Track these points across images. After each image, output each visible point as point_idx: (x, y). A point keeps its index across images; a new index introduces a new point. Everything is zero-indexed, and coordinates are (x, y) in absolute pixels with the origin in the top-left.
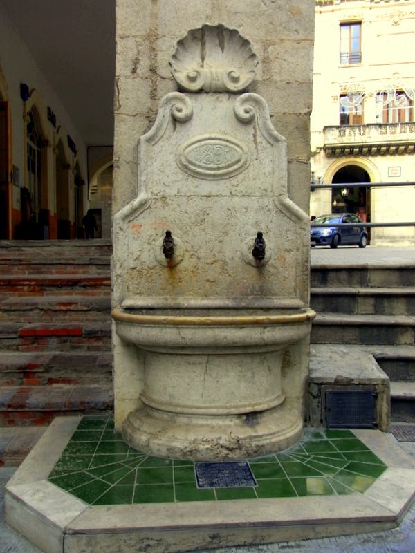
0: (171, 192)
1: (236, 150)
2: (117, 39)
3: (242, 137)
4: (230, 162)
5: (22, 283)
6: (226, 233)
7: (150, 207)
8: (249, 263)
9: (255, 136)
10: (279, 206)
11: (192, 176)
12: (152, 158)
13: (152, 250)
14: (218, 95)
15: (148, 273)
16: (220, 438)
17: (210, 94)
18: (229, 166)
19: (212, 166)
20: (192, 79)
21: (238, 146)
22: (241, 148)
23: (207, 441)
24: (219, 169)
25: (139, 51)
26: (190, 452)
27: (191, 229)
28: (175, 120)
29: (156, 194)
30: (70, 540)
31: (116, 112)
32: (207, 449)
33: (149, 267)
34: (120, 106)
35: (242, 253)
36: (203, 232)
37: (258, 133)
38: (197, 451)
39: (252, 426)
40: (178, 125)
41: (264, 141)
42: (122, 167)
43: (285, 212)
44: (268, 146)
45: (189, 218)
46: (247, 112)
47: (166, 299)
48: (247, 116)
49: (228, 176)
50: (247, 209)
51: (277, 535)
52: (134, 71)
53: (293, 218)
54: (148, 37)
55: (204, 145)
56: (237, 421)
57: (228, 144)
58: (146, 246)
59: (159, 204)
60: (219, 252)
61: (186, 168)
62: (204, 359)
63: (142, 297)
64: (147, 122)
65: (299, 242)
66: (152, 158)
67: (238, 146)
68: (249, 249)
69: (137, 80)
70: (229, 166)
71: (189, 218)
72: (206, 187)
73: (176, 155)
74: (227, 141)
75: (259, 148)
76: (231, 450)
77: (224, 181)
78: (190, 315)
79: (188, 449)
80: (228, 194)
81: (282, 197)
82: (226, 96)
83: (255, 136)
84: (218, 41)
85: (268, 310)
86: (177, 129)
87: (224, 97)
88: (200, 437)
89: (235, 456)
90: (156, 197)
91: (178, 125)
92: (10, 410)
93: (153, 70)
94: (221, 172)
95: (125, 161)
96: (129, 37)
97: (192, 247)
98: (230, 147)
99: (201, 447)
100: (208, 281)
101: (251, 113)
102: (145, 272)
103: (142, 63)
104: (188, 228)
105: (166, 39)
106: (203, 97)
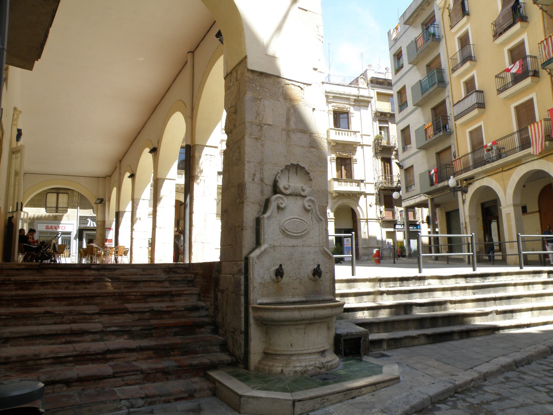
0: (277, 244)
1: (305, 224)
2: (246, 163)
3: (307, 218)
4: (303, 230)
5: (131, 294)
6: (301, 264)
7: (268, 252)
8: (311, 279)
9: (312, 218)
10: (323, 252)
11: (287, 236)
12: (269, 227)
13: (269, 274)
14: (296, 197)
15: (267, 285)
16: (316, 363)
17: (293, 196)
18: (303, 232)
19: (295, 231)
20: (286, 189)
21: (306, 222)
22: (307, 224)
23: (311, 365)
24: (298, 233)
25: (255, 170)
26: (305, 371)
27: (286, 262)
28: (279, 208)
29: (270, 245)
30: (297, 404)
31: (245, 201)
32: (312, 369)
33: (268, 282)
34: (247, 197)
35: (308, 274)
36: (291, 264)
37: (313, 216)
38: (308, 370)
39: (324, 357)
40: (280, 210)
41: (315, 220)
42: (248, 230)
43: (325, 254)
44: (317, 222)
45: (285, 257)
46: (309, 206)
47: (276, 298)
48: (309, 208)
49: (301, 237)
50: (309, 253)
51: (364, 390)
52: (253, 180)
53: (328, 257)
54: (260, 163)
55: (292, 221)
56: (318, 356)
57: (302, 221)
58: (267, 271)
59: (272, 250)
60: (299, 274)
61: (284, 232)
62: (304, 326)
63: (265, 298)
64: (259, 206)
65: (331, 268)
66: (269, 227)
67: (306, 222)
68: (311, 272)
69: (254, 185)
70: (303, 232)
71: (285, 257)
72: (293, 242)
73: (279, 225)
74: (301, 220)
75: (314, 223)
76: (320, 368)
77: (300, 239)
78: (306, 305)
79: (303, 370)
80: (302, 245)
81: (324, 247)
82: (301, 197)
83: (312, 218)
84: (295, 171)
85: (319, 302)
86: (279, 213)
87: (299, 198)
88: (307, 364)
89: (323, 371)
90: (271, 246)
91: (280, 210)
92: (180, 369)
93: (262, 180)
94: (299, 235)
95: (249, 226)
96: (251, 162)
97: (287, 272)
98: (303, 223)
99: (309, 368)
100: (294, 288)
101: (311, 207)
102: (266, 285)
103: (257, 176)
104: (285, 262)
105: (268, 165)
106: (290, 197)
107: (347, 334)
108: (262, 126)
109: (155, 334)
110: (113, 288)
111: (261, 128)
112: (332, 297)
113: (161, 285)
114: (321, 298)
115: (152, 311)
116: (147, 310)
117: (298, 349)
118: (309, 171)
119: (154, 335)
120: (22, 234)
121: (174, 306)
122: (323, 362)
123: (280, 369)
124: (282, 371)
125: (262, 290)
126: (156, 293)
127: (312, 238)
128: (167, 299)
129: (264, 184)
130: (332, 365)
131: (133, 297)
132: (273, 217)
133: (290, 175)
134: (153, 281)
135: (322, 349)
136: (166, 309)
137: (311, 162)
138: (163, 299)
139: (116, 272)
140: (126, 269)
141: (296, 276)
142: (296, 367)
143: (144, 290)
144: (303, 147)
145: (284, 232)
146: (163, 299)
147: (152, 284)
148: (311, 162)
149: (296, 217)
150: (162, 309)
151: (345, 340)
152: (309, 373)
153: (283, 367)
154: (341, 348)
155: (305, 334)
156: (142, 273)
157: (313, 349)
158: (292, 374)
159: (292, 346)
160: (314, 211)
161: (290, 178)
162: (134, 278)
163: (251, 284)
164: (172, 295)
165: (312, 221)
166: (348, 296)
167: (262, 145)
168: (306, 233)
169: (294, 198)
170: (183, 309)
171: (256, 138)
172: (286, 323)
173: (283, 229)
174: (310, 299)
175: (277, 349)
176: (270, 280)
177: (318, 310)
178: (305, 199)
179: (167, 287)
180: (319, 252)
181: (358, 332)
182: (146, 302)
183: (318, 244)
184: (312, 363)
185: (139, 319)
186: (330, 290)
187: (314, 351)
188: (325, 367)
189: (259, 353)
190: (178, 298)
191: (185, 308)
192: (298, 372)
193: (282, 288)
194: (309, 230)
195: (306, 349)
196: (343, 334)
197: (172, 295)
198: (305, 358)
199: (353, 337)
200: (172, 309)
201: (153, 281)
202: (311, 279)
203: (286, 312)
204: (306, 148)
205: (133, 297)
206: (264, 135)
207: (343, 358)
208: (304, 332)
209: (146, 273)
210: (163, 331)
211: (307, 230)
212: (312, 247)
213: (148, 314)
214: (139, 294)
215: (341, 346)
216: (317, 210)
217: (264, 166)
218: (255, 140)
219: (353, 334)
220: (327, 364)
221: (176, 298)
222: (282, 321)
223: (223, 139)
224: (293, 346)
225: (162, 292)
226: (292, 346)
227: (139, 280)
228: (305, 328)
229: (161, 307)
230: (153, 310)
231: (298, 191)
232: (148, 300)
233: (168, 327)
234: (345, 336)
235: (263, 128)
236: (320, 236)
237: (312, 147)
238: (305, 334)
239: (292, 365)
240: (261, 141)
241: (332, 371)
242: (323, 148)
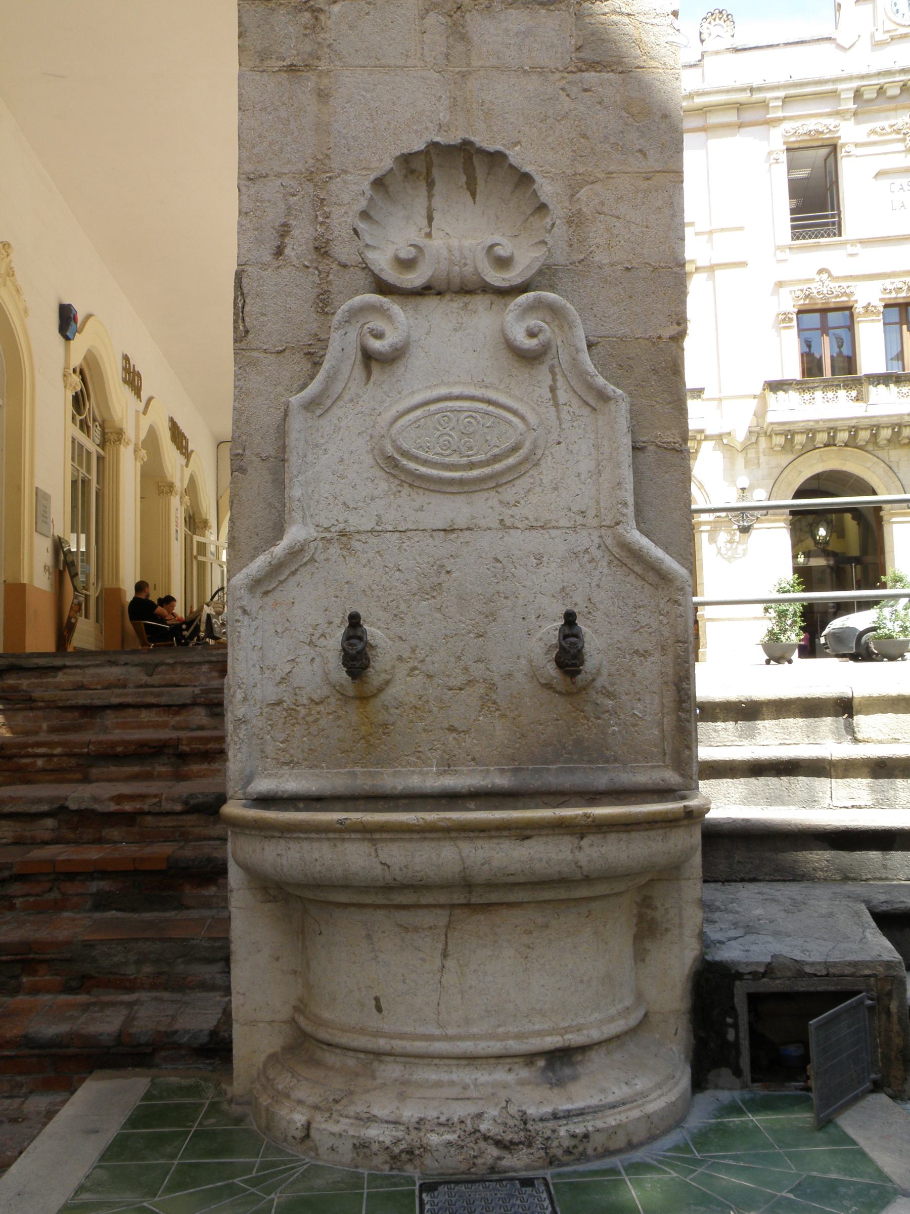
0: (360, 521)
1: (509, 423)
4: (496, 451)
5: (30, 750)
6: (492, 616)
7: (312, 560)
8: (548, 686)
9: (553, 389)
10: (616, 550)
11: (411, 485)
12: (317, 446)
13: (318, 660)
14: (467, 299)
15: (309, 714)
16: (480, 1116)
17: (448, 297)
18: (496, 459)
19: (455, 459)
21: (515, 413)
22: (522, 418)
23: (448, 1125)
24: (472, 466)
26: (410, 1152)
28: (369, 358)
29: (327, 529)
32: (449, 1144)
36: (438, 615)
37: (560, 382)
38: (425, 1148)
41: (575, 402)
44: (586, 411)
46: (532, 334)
47: (354, 775)
49: (494, 482)
50: (539, 558)
52: (279, 252)
53: (651, 577)
59: (334, 550)
62: (441, 918)
65: (666, 633)
66: (317, 446)
67: (515, 413)
70: (496, 459)
74: (489, 402)
75: (564, 415)
76: (506, 1146)
77: (486, 495)
78: (515, 808)
79: (403, 1146)
80: (495, 524)
83: (553, 389)
84: (464, 179)
85: (594, 797)
86: (373, 378)
87: (480, 302)
90: (328, 535)
93: (322, 250)
96: (267, 176)
99: (434, 1139)
100: (452, 729)
101: (541, 337)
103: (295, 232)
105: (350, 177)
106: (430, 303)
107: (769, 965)
108: (321, 10)
109: (20, 900)
110: (13, 733)
111: (317, 18)
112: (671, 777)
113: (178, 718)
114: (601, 781)
115: (60, 811)
116: (45, 808)
117: (408, 1029)
118: (527, 169)
119: (18, 902)
120: (143, 596)
121: (142, 797)
122: (532, 1111)
123: (299, 1118)
124: (308, 1126)
125: (283, 736)
126: (119, 749)
127: (556, 489)
128: (163, 769)
129: (334, 266)
130: (586, 1136)
131: (40, 762)
132: (339, 397)
133: (437, 202)
134: (149, 706)
135: (551, 1042)
136: (113, 807)
137: (584, 136)
138: (148, 768)
139: (57, 679)
140: (88, 666)
141: (466, 669)
142: (372, 1119)
143: (117, 735)
144: (540, 71)
145: (396, 465)
146: (148, 768)
147: (145, 716)
148: (584, 136)
149: (456, 391)
150: (98, 807)
151: (754, 999)
152: (428, 1161)
153: (316, 1108)
154: (731, 1036)
155: (445, 955)
156: (145, 679)
157: (493, 1037)
158: (346, 1153)
159: (379, 1009)
160: (564, 357)
161: (436, 216)
162: (82, 698)
163: (229, 714)
164: (183, 757)
165: (556, 404)
166: (828, 775)
167: (323, 95)
168: (520, 463)
169: (454, 305)
170: (179, 807)
171: (292, 69)
172: (343, 898)
173: (390, 450)
174: (535, 783)
175: (326, 1014)
176: (325, 691)
177: (480, 843)
178: (512, 306)
179: (201, 728)
180: (597, 554)
181: (835, 964)
182: (86, 779)
183: (592, 513)
184: (459, 1111)
185: (18, 842)
186: (663, 738)
187: (496, 1047)
188: (538, 1143)
189: (271, 1022)
190: (205, 766)
191: (186, 803)
192: (375, 1147)
193: (385, 725)
194: (535, 446)
195: (451, 1031)
196: (748, 964)
197: (183, 757)
198: (445, 1077)
199: (802, 986)
200: (138, 805)
201: (149, 706)
202: (548, 686)
203: (306, 845)
204: (558, 75)
205: (40, 762)
206: (329, 46)
207: (744, 1086)
208: (440, 946)
209: (156, 679)
210: (51, 890)
211: (522, 452)
212: (553, 532)
213: (49, 823)
214: (58, 751)
215: (735, 1026)
216: (578, 351)
217: (332, 186)
218: (284, 75)
219: (808, 969)
220: (551, 1124)
221: (195, 767)
222: (332, 886)
223: (780, 279)
224: (385, 1012)
225: (141, 744)
226: (379, 1009)
227: (97, 702)
228: (448, 927)
229: (95, 799)
230: (63, 809)
231: (469, 269)
232: (94, 771)
233: (71, 876)
234: (755, 975)
235: (322, 17)
236: (599, 473)
237: (593, 65)
238: (445, 955)
239: (359, 1107)
240: (314, 78)
241: (581, 1168)
242: (653, 63)
